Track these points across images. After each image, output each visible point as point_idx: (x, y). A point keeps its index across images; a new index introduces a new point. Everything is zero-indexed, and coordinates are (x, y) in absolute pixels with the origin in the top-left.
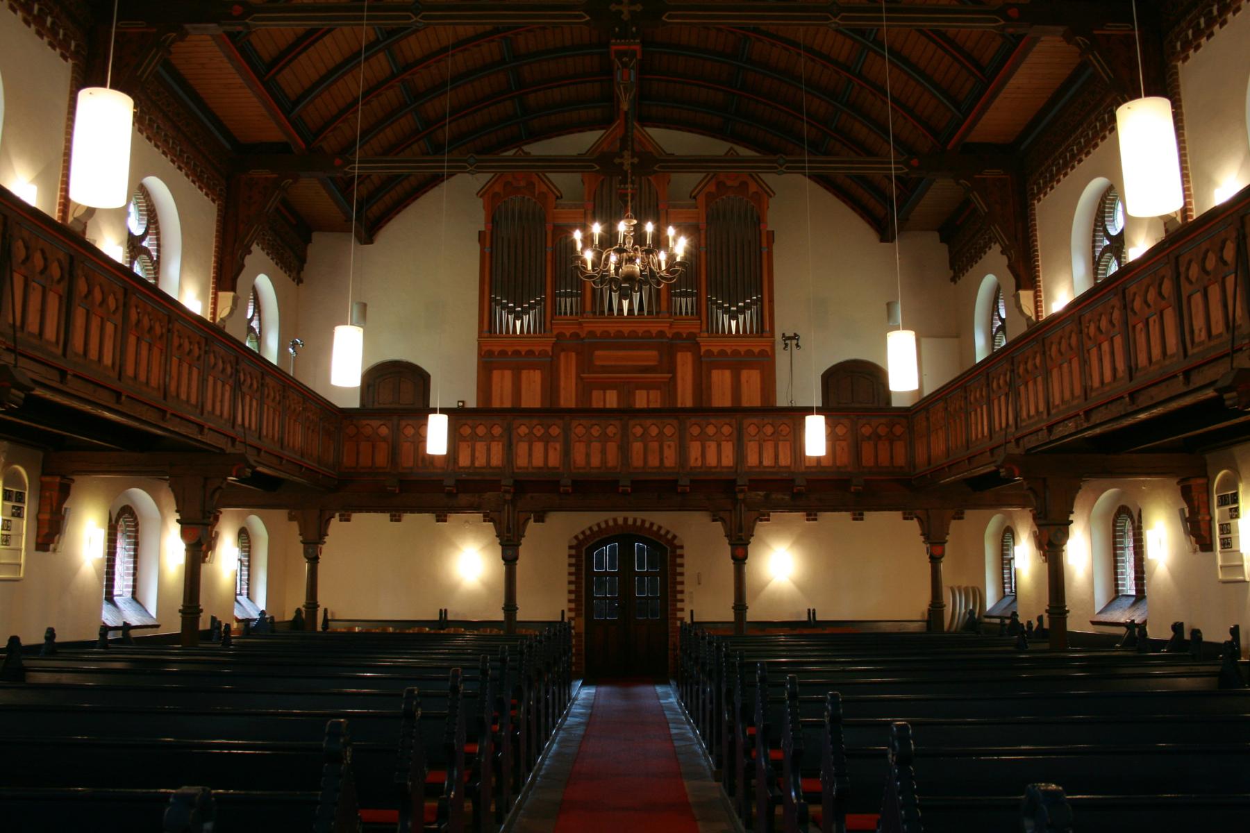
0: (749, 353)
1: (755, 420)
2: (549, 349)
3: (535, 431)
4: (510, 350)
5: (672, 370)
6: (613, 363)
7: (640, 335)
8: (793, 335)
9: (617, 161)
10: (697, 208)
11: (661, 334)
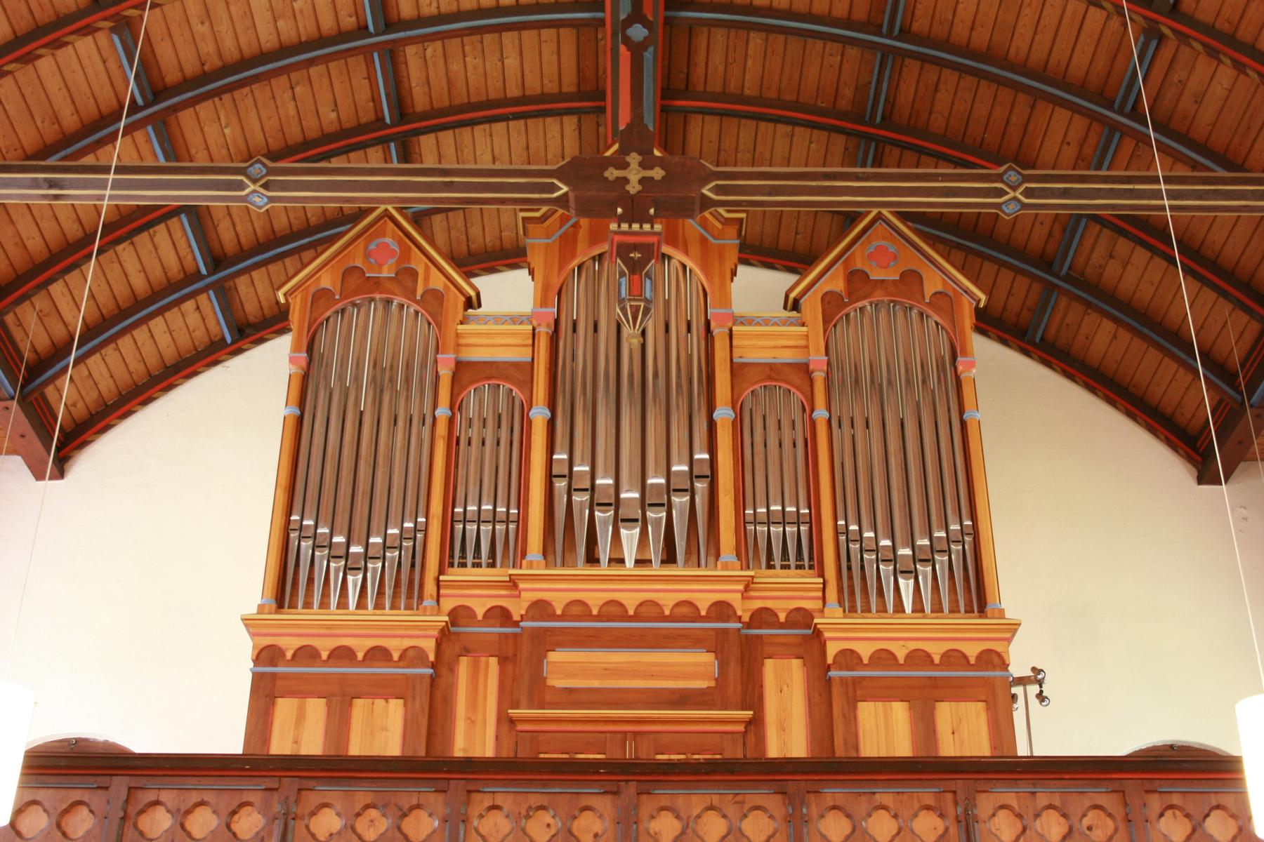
0: (954, 658)
1: (1009, 797)
2: (429, 645)
3: (361, 825)
4: (325, 646)
5: (752, 697)
6: (595, 684)
7: (667, 612)
8: (1030, 673)
9: (612, 174)
10: (803, 325)
11: (722, 610)
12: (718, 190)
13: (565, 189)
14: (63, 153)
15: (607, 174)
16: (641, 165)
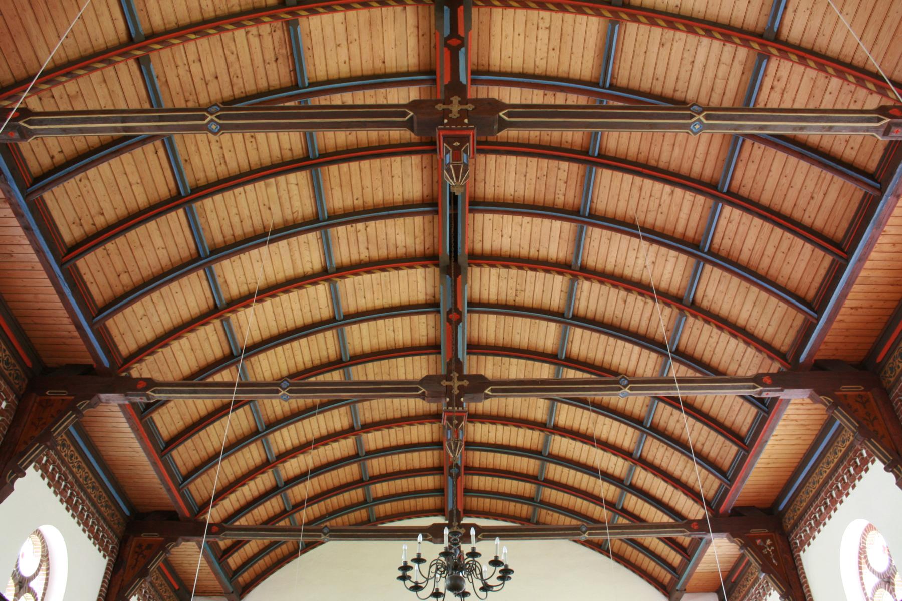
12: (509, 115)
13: (412, 114)
14: (200, 378)
15: (442, 383)
16: (460, 103)
